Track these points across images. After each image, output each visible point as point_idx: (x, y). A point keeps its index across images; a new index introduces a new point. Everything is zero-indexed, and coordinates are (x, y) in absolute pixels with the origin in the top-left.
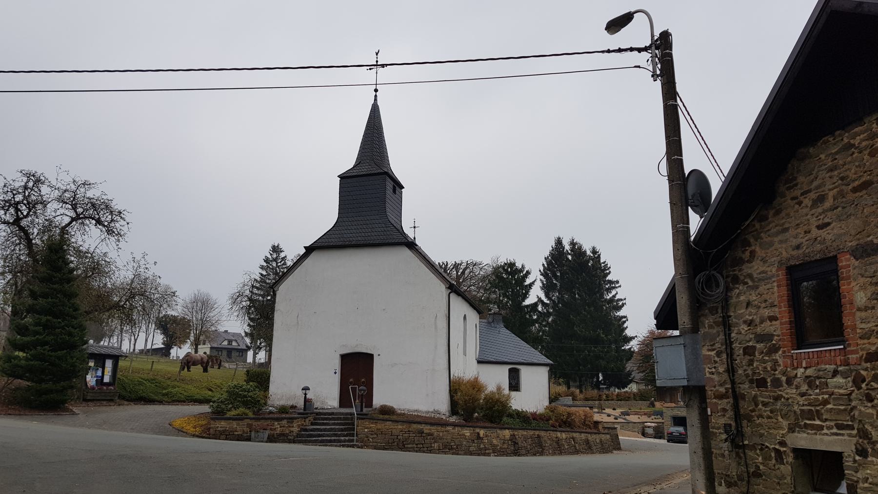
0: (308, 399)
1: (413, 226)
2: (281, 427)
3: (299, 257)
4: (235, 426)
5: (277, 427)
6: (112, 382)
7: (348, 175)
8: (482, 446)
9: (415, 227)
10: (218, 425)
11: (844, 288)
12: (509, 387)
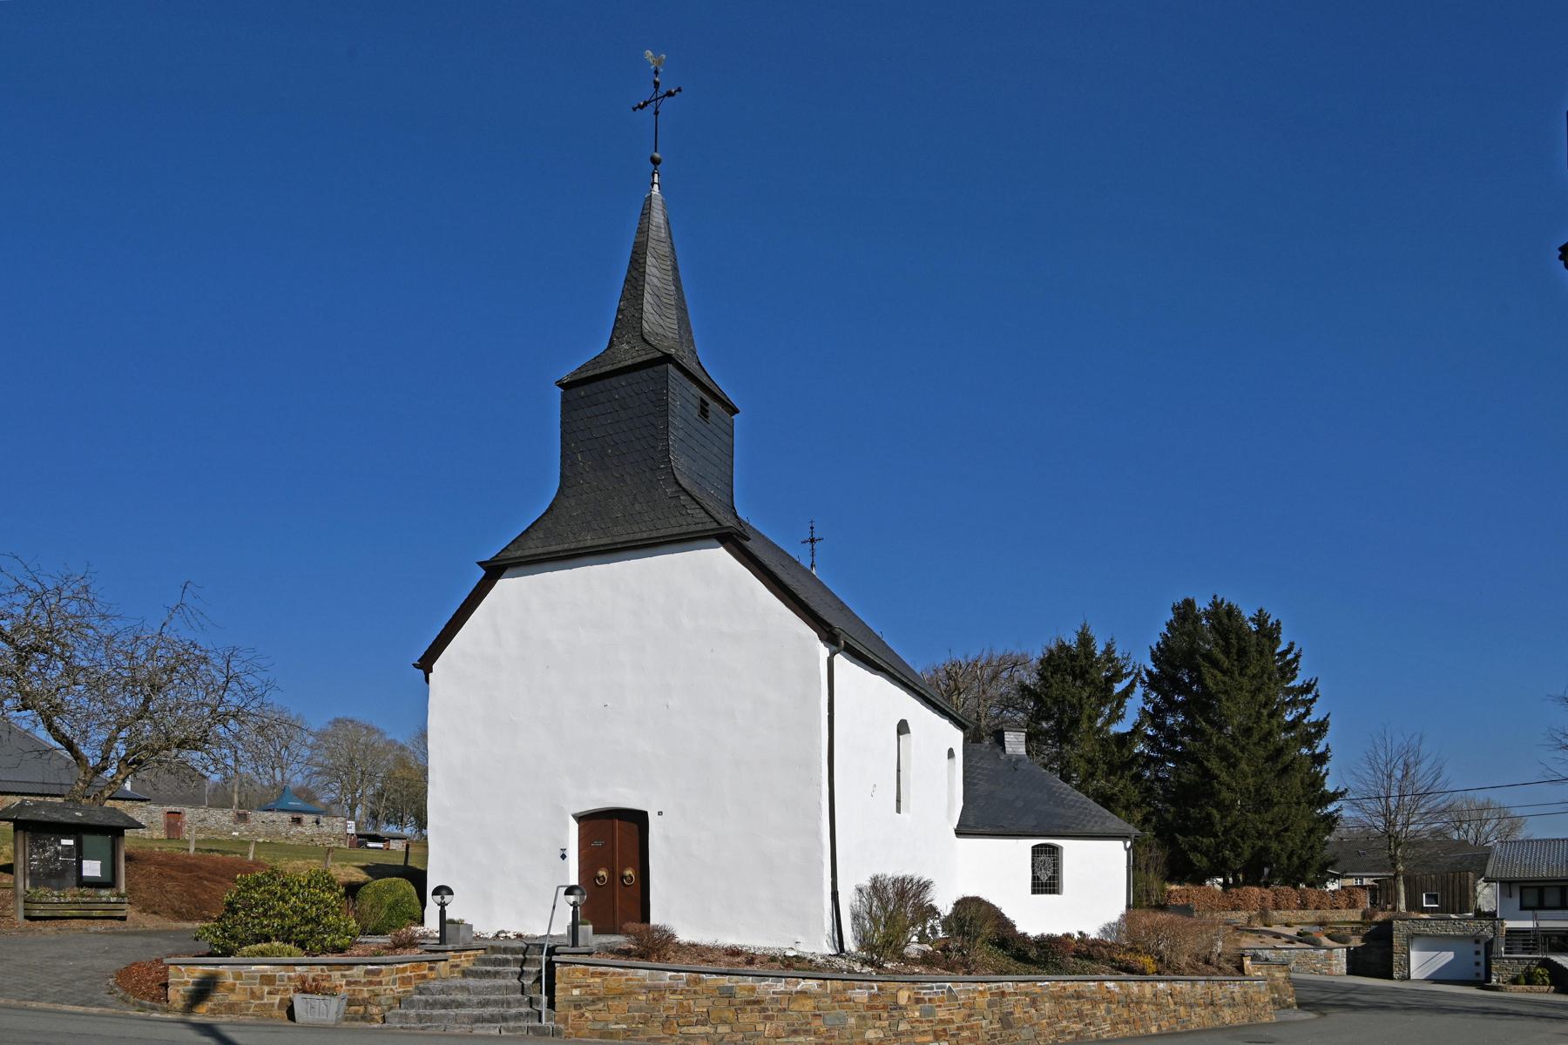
0: (452, 922)
1: (807, 537)
2: (348, 983)
3: (1461, 933)
4: (231, 981)
5: (338, 983)
6: (84, 880)
7: (584, 375)
8: (903, 1027)
9: (812, 541)
10: (186, 979)
11: (1418, 827)
12: (1050, 893)
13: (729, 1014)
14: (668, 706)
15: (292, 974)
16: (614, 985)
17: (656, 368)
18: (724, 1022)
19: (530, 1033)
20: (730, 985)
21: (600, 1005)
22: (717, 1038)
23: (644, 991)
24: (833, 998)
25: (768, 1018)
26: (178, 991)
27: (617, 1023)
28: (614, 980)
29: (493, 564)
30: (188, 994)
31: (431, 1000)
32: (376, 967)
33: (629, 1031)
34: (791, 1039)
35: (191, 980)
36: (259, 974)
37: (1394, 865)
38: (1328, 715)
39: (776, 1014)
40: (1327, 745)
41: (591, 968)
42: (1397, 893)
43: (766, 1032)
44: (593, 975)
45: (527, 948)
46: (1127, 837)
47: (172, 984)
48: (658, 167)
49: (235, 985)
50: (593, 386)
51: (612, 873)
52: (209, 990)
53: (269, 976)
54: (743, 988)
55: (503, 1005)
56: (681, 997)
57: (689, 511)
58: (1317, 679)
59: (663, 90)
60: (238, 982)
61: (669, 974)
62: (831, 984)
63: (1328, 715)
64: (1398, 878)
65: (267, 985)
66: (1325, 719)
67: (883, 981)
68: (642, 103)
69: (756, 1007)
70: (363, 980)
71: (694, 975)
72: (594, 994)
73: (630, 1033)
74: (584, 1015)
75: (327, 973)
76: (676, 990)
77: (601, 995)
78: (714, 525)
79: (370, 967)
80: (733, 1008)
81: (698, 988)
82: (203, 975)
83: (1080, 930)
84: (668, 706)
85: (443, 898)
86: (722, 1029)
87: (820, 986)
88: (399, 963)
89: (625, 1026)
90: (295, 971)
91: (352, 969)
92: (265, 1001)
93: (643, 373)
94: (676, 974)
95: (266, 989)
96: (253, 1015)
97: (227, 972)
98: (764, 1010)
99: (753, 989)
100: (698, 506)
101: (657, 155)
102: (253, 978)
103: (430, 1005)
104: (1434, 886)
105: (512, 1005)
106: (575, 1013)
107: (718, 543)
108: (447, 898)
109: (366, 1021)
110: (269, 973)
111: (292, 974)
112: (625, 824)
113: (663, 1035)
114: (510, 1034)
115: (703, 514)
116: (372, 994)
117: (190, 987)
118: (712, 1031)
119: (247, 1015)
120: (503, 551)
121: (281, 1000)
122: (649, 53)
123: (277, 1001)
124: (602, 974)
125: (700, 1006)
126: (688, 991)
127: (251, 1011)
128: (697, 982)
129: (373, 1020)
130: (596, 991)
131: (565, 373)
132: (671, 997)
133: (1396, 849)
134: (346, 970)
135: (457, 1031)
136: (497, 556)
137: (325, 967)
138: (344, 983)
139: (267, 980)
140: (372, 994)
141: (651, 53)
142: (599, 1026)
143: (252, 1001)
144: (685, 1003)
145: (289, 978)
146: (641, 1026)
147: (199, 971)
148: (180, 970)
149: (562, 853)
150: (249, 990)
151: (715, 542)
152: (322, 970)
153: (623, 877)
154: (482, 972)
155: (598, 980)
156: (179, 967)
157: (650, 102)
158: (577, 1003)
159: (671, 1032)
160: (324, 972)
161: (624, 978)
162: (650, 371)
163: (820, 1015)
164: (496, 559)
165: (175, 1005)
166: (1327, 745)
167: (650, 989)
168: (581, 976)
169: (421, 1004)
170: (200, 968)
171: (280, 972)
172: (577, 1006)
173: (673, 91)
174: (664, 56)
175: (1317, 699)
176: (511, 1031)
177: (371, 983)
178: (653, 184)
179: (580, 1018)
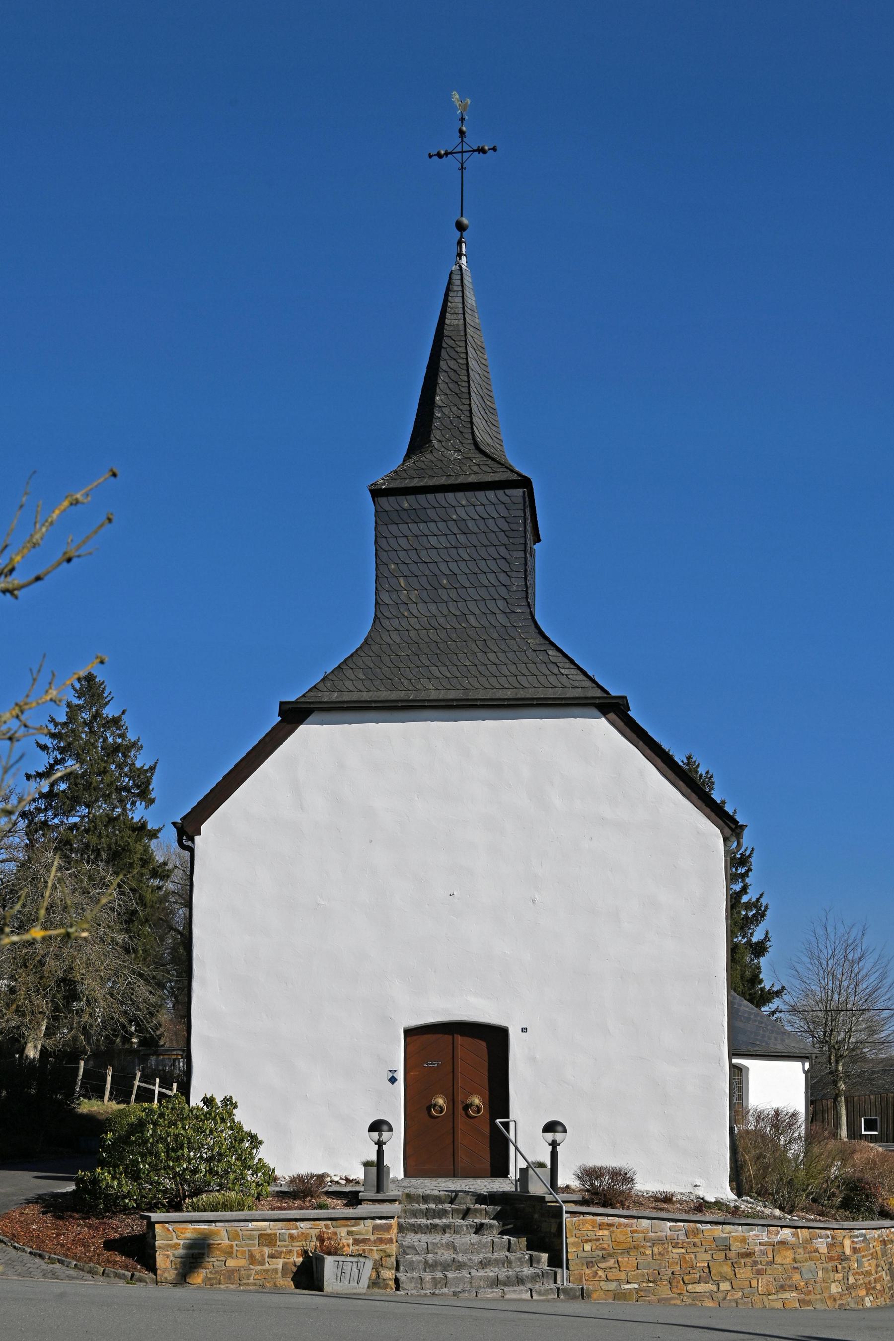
2: (356, 1242)
13: (727, 1269)
14: (534, 901)
15: (294, 1232)
16: (621, 1238)
17: (508, 491)
18: (725, 1279)
19: (562, 1297)
20: (724, 1235)
21: (611, 1262)
22: (720, 1296)
23: (649, 1244)
24: (805, 1248)
25: (759, 1272)
26: (168, 1257)
27: (628, 1283)
28: (621, 1232)
29: (299, 706)
30: (179, 1260)
31: (431, 1261)
32: (384, 1221)
33: (641, 1291)
34: (780, 1296)
35: (182, 1242)
36: (256, 1233)
37: (835, 1083)
38: (761, 895)
39: (764, 1267)
40: (767, 933)
41: (598, 1218)
42: (838, 1118)
43: (760, 1289)
44: (601, 1226)
45: (456, 1196)
46: (807, 1058)
47: (160, 1248)
48: (464, 233)
49: (232, 1246)
50: (421, 498)
51: (452, 1101)
52: (203, 1254)
53: (269, 1235)
54: (736, 1239)
55: (503, 1264)
56: (683, 1251)
57: (563, 671)
58: (753, 850)
59: (472, 141)
60: (234, 1243)
61: (669, 1224)
62: (801, 1232)
63: (761, 895)
64: (839, 1099)
65: (268, 1246)
66: (758, 900)
67: (833, 1229)
68: (443, 152)
69: (748, 1260)
70: (372, 1238)
71: (692, 1224)
72: (604, 1249)
73: (642, 1293)
74: (597, 1274)
75: (332, 1230)
76: (677, 1243)
77: (611, 1250)
78: (599, 693)
79: (378, 1222)
80: (729, 1262)
81: (696, 1240)
82: (195, 1236)
83: (364, 1160)
84: (534, 901)
85: (380, 1135)
86: (725, 1286)
87: (793, 1235)
88: (381, 1218)
89: (636, 1286)
90: (297, 1228)
91: (359, 1225)
92: (267, 1266)
93: (491, 494)
94: (674, 1224)
95: (267, 1251)
96: (255, 1284)
97: (221, 1234)
98: (755, 1263)
99: (744, 1240)
100: (572, 666)
101: (465, 221)
102: (251, 1238)
103: (431, 1266)
104: (873, 1109)
105: (514, 1265)
106: (588, 1271)
107: (598, 713)
108: (559, 1136)
109: (379, 1287)
110: (269, 1231)
111: (294, 1232)
112: (468, 1040)
113: (672, 1295)
114: (541, 1298)
115: (582, 677)
116: (383, 1254)
117: (181, 1251)
118: (715, 1288)
119: (248, 1284)
120: (310, 690)
121: (284, 1264)
122: (456, 96)
123: (280, 1266)
124: (610, 1225)
125: (702, 1259)
126: (688, 1243)
127: (251, 1281)
128: (696, 1232)
129: (386, 1286)
130: (606, 1246)
131: (379, 476)
132: (674, 1251)
133: (837, 1062)
134: (353, 1226)
135: (490, 1296)
136: (304, 696)
137: (329, 1222)
138: (351, 1241)
139: (267, 1239)
140: (383, 1254)
141: (457, 96)
142: (613, 1286)
143: (252, 1267)
144: (687, 1256)
145: (291, 1237)
146: (651, 1285)
147: (190, 1231)
148: (168, 1230)
149: (391, 1075)
150: (247, 1252)
151: (596, 712)
152: (327, 1227)
153: (467, 1107)
154: (427, 1226)
155: (606, 1232)
156: (167, 1225)
157: (451, 153)
158: (589, 1260)
159: (679, 1292)
160: (329, 1228)
161: (629, 1229)
162: (500, 493)
163: (797, 1268)
164: (303, 700)
165: (166, 1275)
166: (767, 933)
167: (654, 1242)
168: (590, 1228)
169: (421, 1266)
170: (190, 1226)
171: (279, 1228)
172: (589, 1264)
173: (486, 148)
174: (469, 101)
175: (750, 874)
176: (544, 1295)
177: (381, 1241)
178: (460, 255)
179: (594, 1277)
